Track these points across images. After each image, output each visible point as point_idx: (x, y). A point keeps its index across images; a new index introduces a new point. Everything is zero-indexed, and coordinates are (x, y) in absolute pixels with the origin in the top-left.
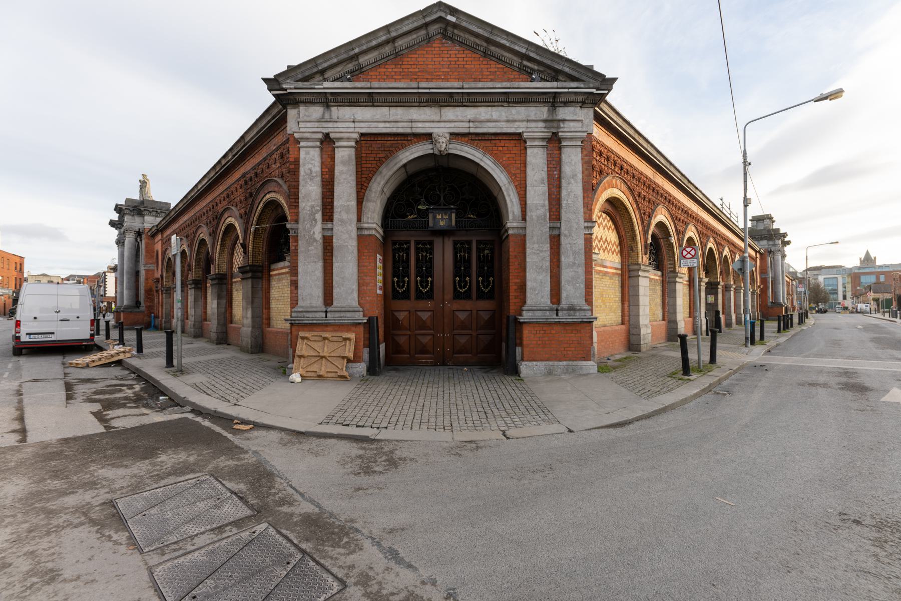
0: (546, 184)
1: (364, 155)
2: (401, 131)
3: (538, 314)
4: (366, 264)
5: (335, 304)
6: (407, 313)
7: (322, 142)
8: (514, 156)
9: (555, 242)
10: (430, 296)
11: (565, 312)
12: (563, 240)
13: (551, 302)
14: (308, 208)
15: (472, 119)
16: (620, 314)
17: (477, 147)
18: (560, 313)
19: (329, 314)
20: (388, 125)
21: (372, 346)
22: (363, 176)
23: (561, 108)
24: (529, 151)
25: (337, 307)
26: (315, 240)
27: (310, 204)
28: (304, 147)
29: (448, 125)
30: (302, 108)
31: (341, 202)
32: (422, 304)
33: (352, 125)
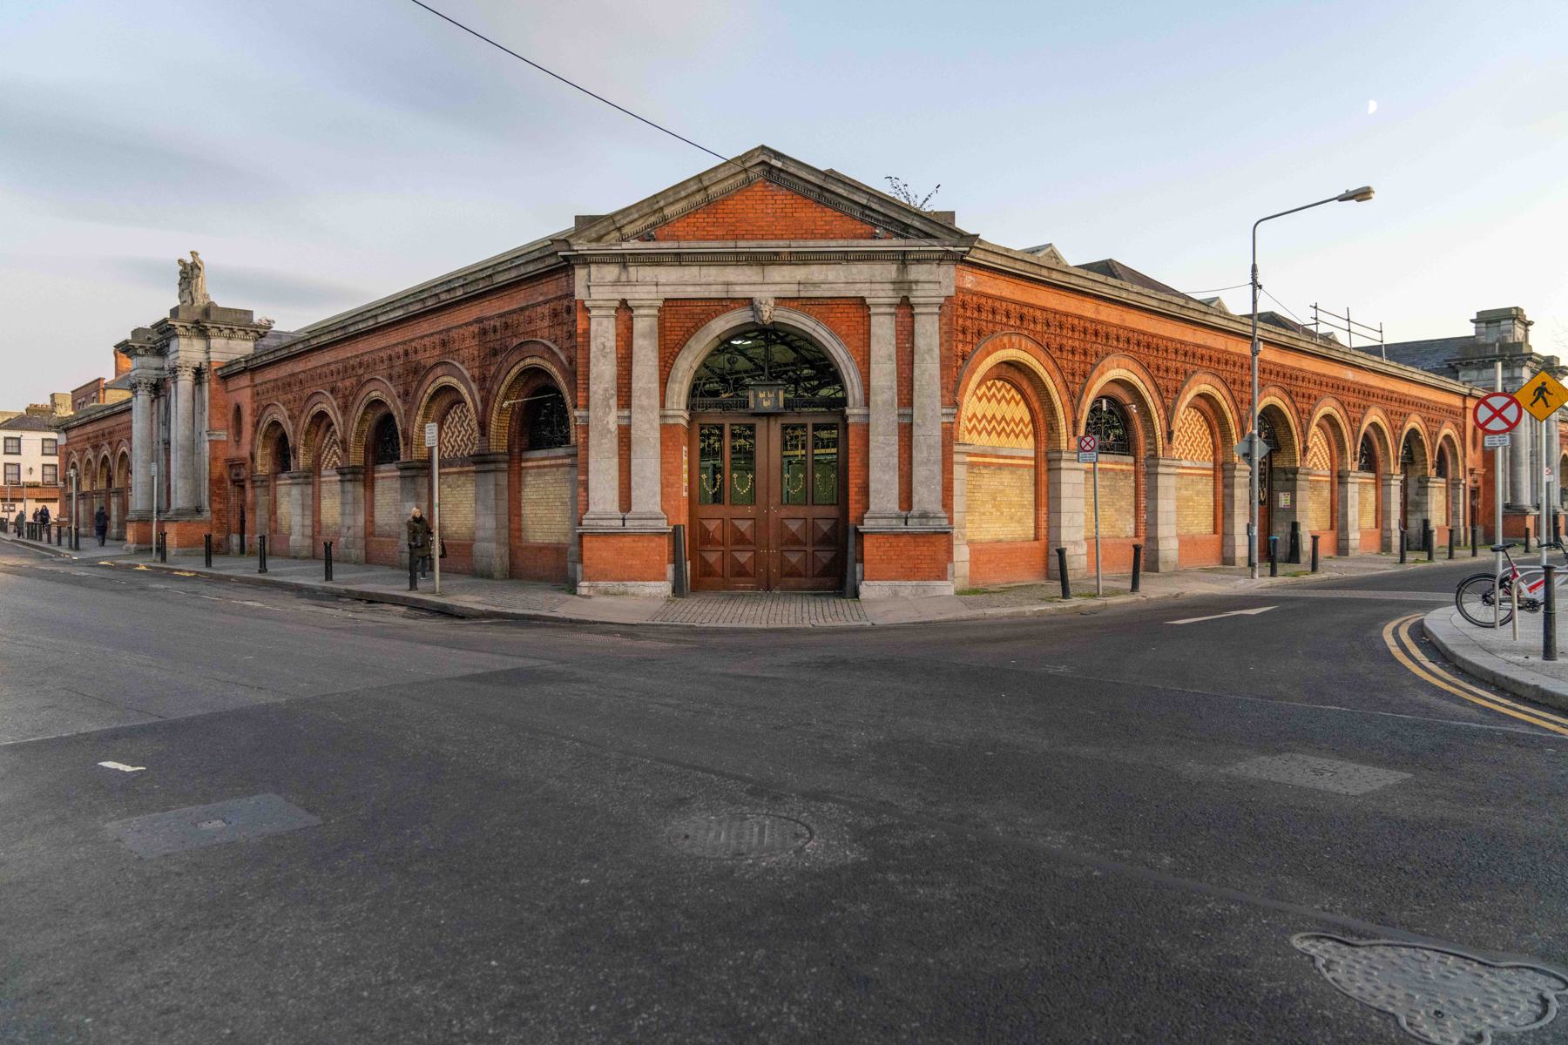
0: (895, 359)
1: (668, 324)
2: (713, 295)
3: (883, 522)
4: (671, 460)
5: (633, 509)
6: (719, 521)
7: (617, 309)
8: (855, 324)
9: (906, 433)
11: (916, 520)
12: (916, 432)
13: (900, 508)
15: (802, 281)
16: (1033, 525)
17: (809, 314)
18: (909, 522)
19: (627, 523)
20: (698, 288)
21: (676, 560)
22: (667, 350)
23: (913, 266)
24: (874, 319)
25: (636, 513)
26: (609, 431)
27: (602, 386)
28: (595, 316)
29: (773, 288)
30: (593, 268)
31: (640, 385)
32: (738, 511)
33: (654, 289)
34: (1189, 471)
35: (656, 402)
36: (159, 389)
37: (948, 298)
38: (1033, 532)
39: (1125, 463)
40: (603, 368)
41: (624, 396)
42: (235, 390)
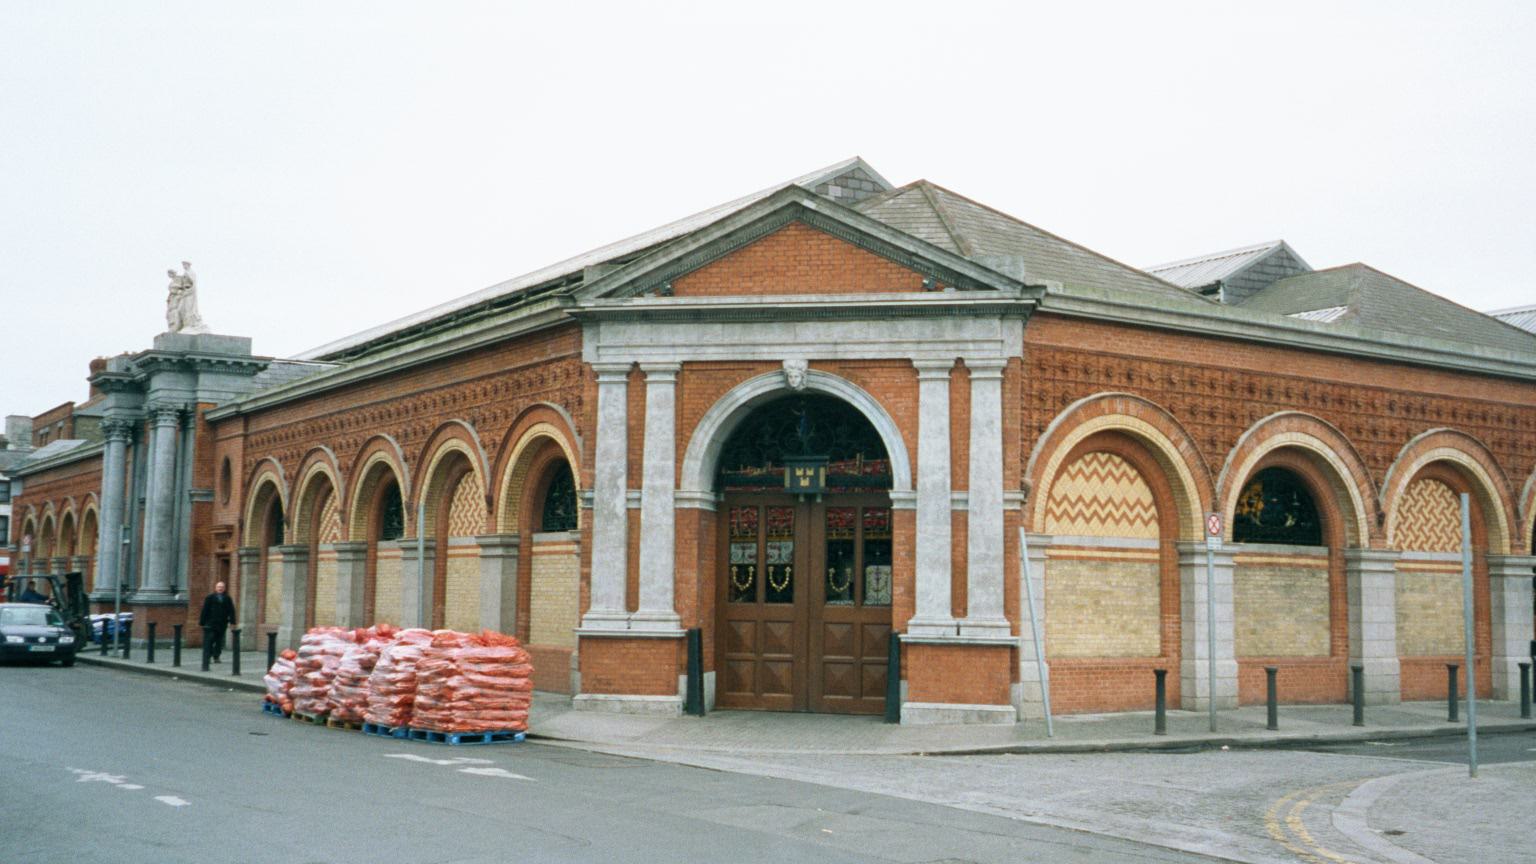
6: (849, 627)
10: (787, 596)
12: (972, 521)
14: (608, 470)
20: (721, 350)
24: (923, 386)
26: (616, 516)
34: (1427, 566)
35: (671, 483)
36: (136, 434)
37: (1011, 360)
38: (1157, 646)
39: (1313, 556)
40: (612, 441)
41: (634, 473)
42: (227, 439)
